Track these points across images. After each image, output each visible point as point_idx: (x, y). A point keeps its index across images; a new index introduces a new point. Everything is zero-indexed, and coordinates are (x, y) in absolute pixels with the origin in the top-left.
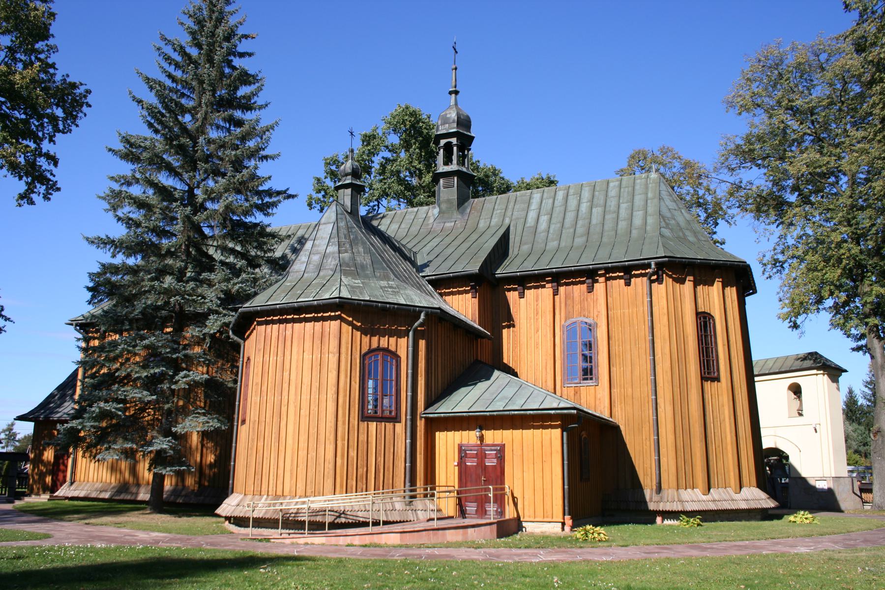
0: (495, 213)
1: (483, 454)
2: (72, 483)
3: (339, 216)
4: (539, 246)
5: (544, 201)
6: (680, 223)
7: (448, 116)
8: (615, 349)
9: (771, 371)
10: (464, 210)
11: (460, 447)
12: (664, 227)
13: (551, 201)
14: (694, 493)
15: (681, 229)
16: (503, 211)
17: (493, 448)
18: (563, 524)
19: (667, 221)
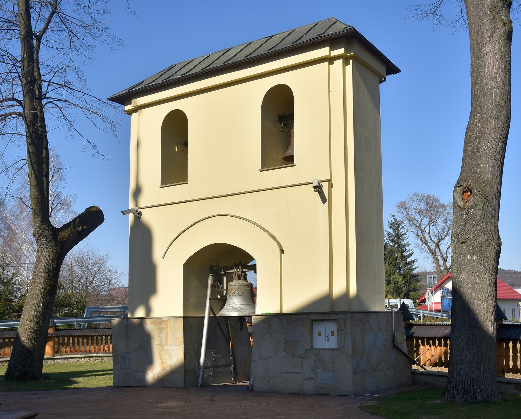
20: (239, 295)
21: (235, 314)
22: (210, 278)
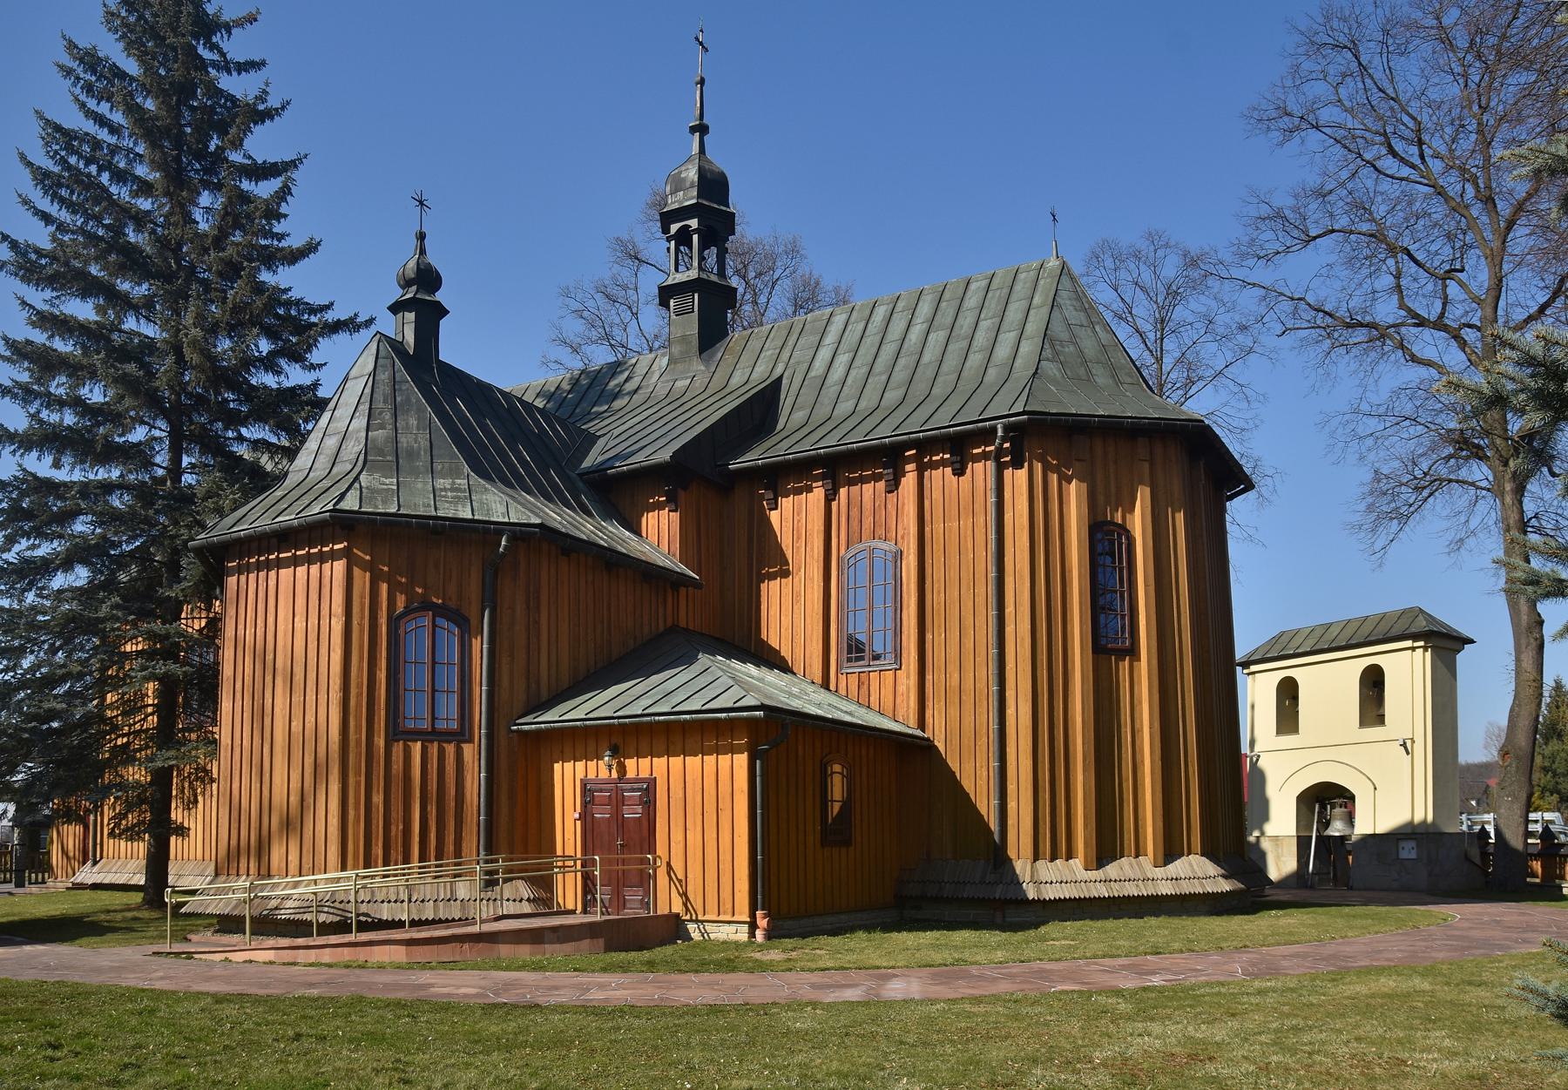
0: (762, 356)
1: (620, 797)
2: (95, 863)
3: (381, 361)
4: (822, 411)
5: (849, 328)
6: (1086, 351)
7: (682, 176)
8: (935, 598)
9: (1333, 645)
10: (711, 356)
11: (584, 784)
12: (1048, 360)
13: (861, 326)
14: (1140, 865)
15: (1085, 362)
16: (778, 351)
17: (636, 786)
18: (753, 926)
19: (1058, 347)
20: (1341, 819)
21: (1337, 834)
22: (1317, 806)
